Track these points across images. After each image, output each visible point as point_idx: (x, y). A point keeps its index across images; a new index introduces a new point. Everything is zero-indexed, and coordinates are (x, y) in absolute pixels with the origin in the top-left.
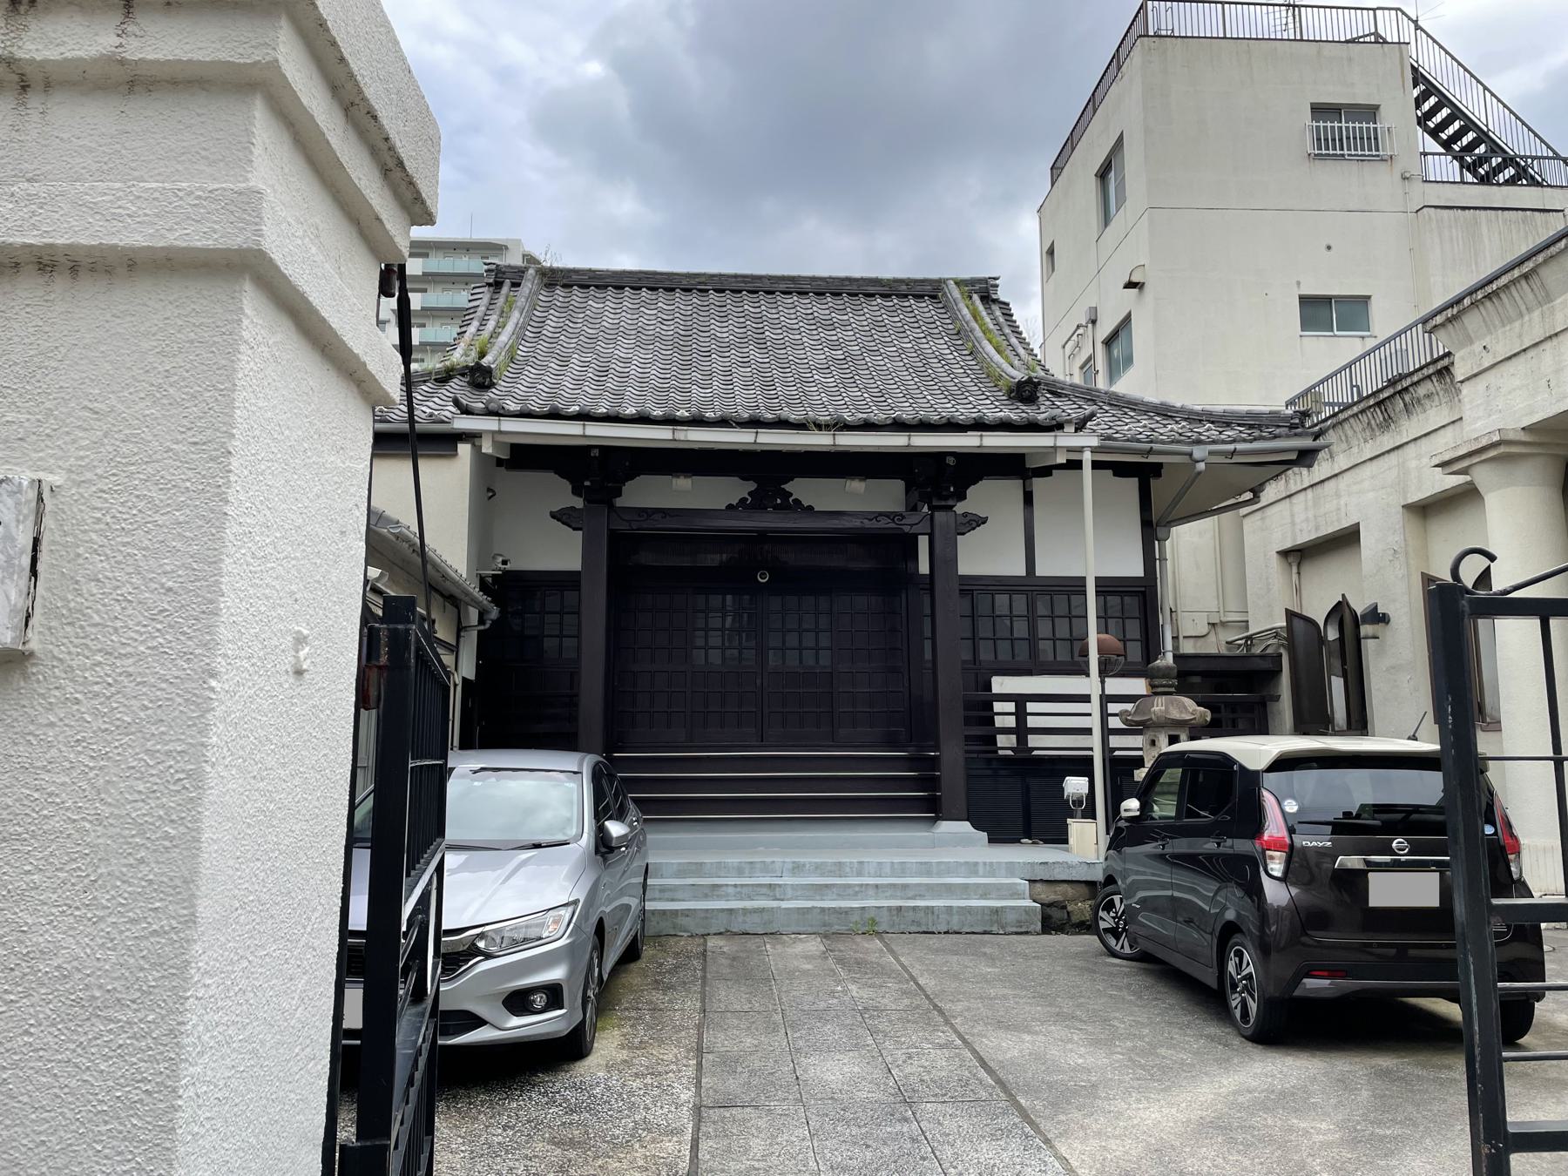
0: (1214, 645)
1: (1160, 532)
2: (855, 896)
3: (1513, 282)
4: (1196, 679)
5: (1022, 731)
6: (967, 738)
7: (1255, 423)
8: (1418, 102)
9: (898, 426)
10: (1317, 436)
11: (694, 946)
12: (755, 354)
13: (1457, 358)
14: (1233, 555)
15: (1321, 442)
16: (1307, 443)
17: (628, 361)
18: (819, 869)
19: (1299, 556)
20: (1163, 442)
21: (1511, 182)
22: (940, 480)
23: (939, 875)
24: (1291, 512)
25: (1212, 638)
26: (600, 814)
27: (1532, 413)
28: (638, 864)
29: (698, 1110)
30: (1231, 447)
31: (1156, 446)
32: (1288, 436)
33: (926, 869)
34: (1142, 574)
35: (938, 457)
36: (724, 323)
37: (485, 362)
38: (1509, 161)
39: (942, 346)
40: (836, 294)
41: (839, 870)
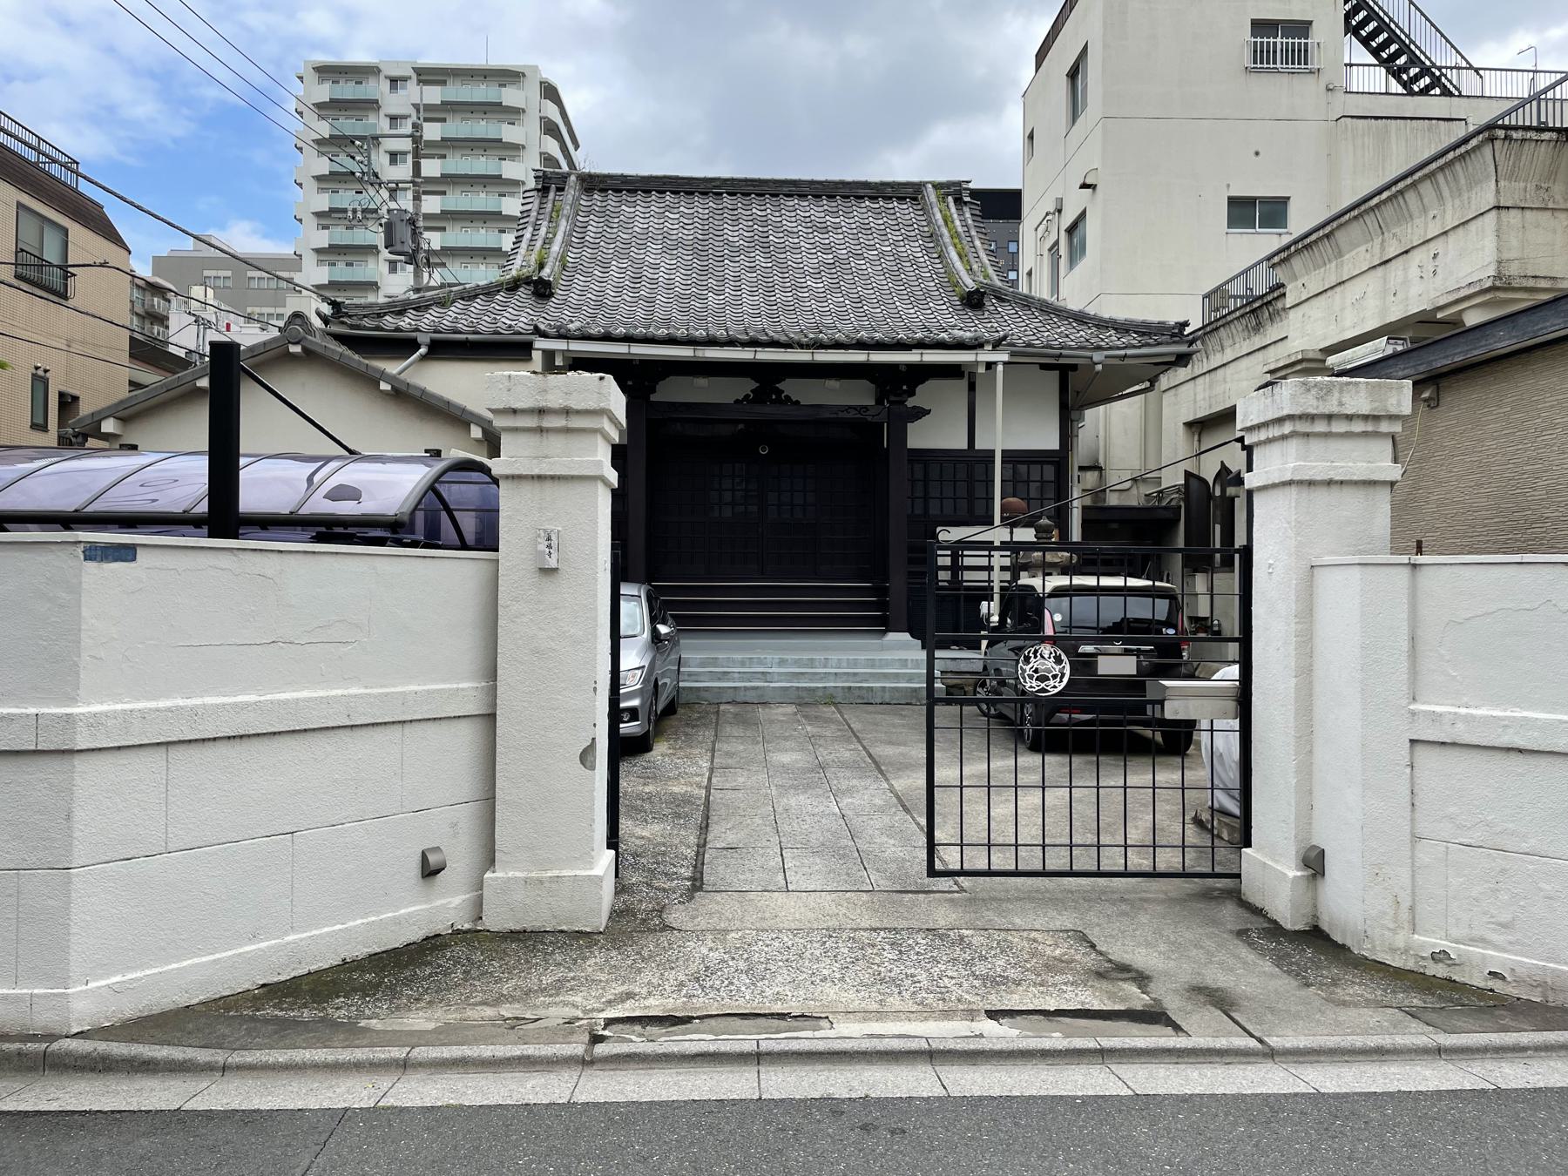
0: (1134, 499)
1: (1074, 415)
2: (821, 680)
3: (1320, 239)
4: (1115, 526)
5: (956, 568)
6: (910, 573)
7: (1147, 330)
8: (1348, 16)
9: (861, 345)
10: (1191, 343)
11: (712, 709)
12: (761, 260)
13: (1289, 289)
14: (1151, 428)
15: (1194, 347)
16: (1183, 348)
17: (656, 267)
18: (797, 663)
19: (1200, 426)
20: (1070, 348)
21: (1425, 92)
22: (896, 385)
23: (881, 667)
24: (1187, 397)
25: (1134, 491)
26: (654, 620)
27: (1325, 339)
28: (674, 656)
29: (712, 770)
30: (1122, 352)
31: (1064, 352)
32: (1168, 344)
33: (871, 663)
34: (1057, 447)
35: (893, 367)
36: (736, 225)
37: (545, 273)
38: (1425, 71)
39: (915, 249)
40: (831, 197)
41: (811, 663)
